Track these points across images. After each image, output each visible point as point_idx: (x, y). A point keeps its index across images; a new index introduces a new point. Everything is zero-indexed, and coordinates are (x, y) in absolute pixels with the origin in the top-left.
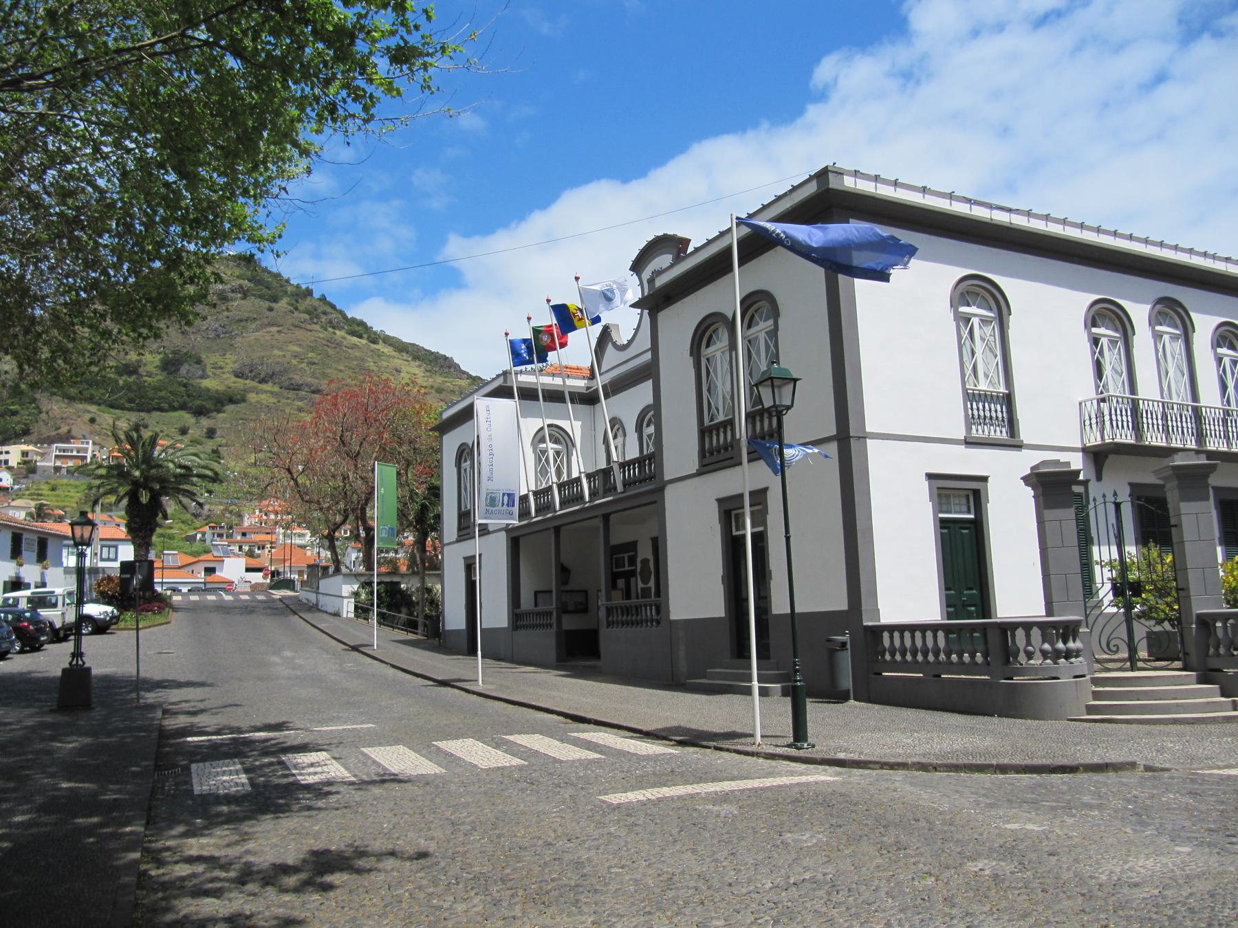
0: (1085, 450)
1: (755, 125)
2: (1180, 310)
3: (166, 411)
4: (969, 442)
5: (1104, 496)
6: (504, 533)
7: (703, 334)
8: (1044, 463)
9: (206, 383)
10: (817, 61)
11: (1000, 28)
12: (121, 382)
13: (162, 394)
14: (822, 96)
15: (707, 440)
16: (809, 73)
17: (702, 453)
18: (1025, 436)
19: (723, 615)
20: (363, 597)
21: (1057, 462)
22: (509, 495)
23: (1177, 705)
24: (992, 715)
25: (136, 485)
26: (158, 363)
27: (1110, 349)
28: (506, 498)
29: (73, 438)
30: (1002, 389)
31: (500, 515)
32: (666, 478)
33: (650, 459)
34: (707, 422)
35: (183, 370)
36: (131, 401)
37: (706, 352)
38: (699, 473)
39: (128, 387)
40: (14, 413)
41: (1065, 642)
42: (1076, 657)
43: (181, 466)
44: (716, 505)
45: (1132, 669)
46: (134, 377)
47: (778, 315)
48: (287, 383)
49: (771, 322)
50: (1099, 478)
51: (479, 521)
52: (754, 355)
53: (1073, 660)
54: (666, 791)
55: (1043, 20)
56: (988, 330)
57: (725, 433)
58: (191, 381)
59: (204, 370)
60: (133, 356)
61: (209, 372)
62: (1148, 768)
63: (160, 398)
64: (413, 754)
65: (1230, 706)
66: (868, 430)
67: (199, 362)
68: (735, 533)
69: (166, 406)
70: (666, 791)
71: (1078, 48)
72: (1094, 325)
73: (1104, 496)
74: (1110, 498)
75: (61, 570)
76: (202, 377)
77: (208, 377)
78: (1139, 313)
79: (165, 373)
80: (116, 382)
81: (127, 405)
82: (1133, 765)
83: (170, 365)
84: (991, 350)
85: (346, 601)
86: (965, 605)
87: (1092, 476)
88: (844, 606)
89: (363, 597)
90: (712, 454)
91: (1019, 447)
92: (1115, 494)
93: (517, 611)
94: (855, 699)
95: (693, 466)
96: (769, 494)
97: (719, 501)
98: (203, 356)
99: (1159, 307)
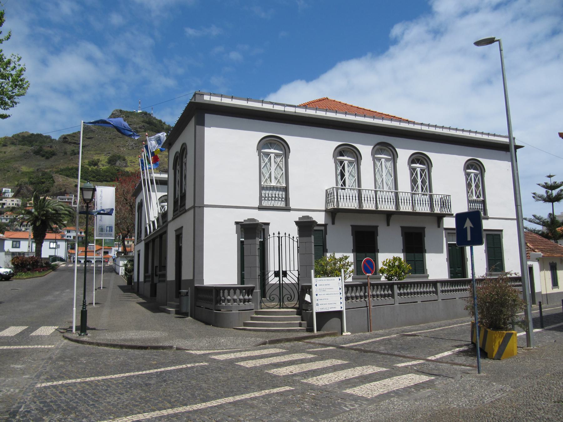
0: (327, 211)
1: (365, 54)
2: (391, 148)
3: (109, 182)
4: (261, 208)
5: (274, 234)
8: (304, 217)
9: (127, 169)
10: (392, 27)
11: (477, 10)
12: (90, 169)
13: (107, 174)
14: (395, 42)
16: (389, 32)
18: (292, 205)
20: (129, 266)
21: (308, 217)
22: (110, 227)
23: (274, 324)
24: (210, 325)
25: (36, 219)
26: (106, 160)
27: (348, 166)
28: (108, 228)
29: (67, 194)
30: (284, 185)
31: (107, 235)
35: (118, 163)
36: (94, 177)
39: (93, 171)
40: (43, 183)
41: (248, 296)
42: (248, 302)
43: (54, 210)
45: (279, 308)
46: (96, 167)
48: (162, 169)
50: (333, 223)
51: (96, 238)
53: (247, 303)
55: (497, 7)
56: (278, 160)
58: (121, 168)
59: (126, 163)
60: (96, 158)
61: (129, 164)
62: (178, 349)
63: (107, 176)
65: (298, 325)
66: (205, 203)
67: (124, 160)
69: (109, 179)
71: (514, 20)
72: (342, 155)
73: (274, 234)
74: (277, 235)
75: (4, 253)
76: (126, 166)
77: (128, 166)
78: (366, 150)
79: (109, 165)
80: (88, 169)
81: (92, 179)
82: (171, 347)
83: (112, 161)
84: (280, 168)
85: (121, 268)
86: (457, 273)
87: (330, 223)
89: (129, 266)
91: (289, 210)
92: (279, 233)
93: (147, 274)
94: (191, 316)
98: (126, 157)
99: (378, 147)
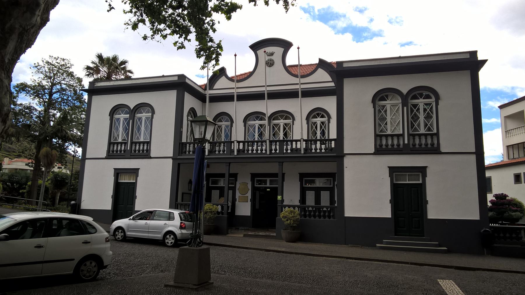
33: (224, 144)
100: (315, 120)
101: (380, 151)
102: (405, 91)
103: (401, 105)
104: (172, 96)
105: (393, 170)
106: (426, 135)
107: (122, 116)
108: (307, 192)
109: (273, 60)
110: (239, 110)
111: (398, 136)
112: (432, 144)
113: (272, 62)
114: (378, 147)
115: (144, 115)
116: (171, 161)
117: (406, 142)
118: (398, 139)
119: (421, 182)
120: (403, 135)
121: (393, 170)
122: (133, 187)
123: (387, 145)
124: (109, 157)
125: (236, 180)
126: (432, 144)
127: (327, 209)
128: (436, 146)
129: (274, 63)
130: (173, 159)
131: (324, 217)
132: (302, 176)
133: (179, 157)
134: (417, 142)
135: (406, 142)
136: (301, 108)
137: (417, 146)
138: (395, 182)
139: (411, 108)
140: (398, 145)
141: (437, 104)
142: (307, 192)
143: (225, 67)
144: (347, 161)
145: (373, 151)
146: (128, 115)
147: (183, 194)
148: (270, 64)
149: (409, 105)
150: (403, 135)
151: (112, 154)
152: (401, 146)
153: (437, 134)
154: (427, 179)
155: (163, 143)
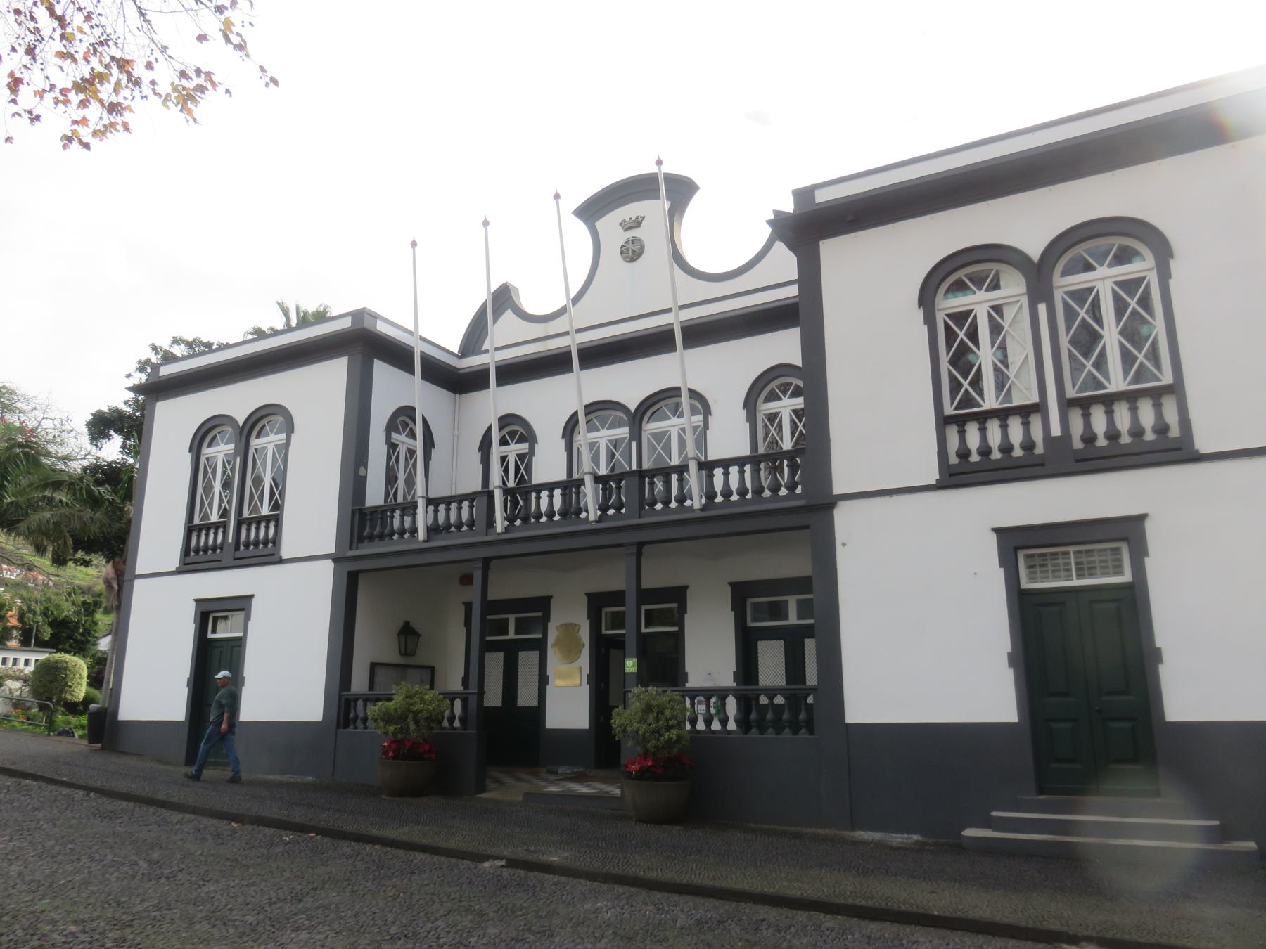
6: (285, 554)
7: (205, 434)
15: (194, 539)
17: (186, 551)
19: (183, 718)
32: (838, 489)
33: (472, 501)
34: (197, 521)
37: (207, 452)
38: (179, 572)
44: (194, 603)
47: (293, 432)
49: (284, 436)
52: (258, 462)
54: (1176, 844)
57: (216, 534)
64: (274, 816)
68: (210, 636)
70: (1176, 844)
88: (535, 703)
90: (197, 552)
95: (174, 562)
96: (254, 600)
97: (197, 601)
100: (772, 407)
101: (958, 474)
102: (1034, 248)
103: (1024, 301)
104: (332, 376)
105: (1014, 542)
106: (1131, 398)
107: (220, 451)
108: (762, 645)
109: (640, 241)
110: (546, 404)
111: (1025, 412)
112: (1161, 429)
113: (636, 247)
114: (953, 460)
115: (267, 442)
116: (329, 566)
117: (1056, 430)
118: (1026, 424)
119: (1126, 577)
120: (1038, 408)
121: (1014, 542)
122: (235, 648)
123: (985, 451)
124: (187, 567)
125: (546, 618)
126: (1161, 429)
127: (771, 698)
128: (1175, 432)
129: (642, 248)
130: (337, 559)
131: (778, 726)
132: (741, 593)
133: (350, 553)
134: (1099, 422)
135: (1056, 430)
136: (725, 372)
137: (1102, 442)
138: (1026, 584)
139: (1067, 306)
140: (1028, 446)
141: (1164, 275)
142: (762, 645)
143: (513, 282)
144: (845, 520)
145: (931, 475)
146: (232, 446)
147: (373, 666)
148: (632, 252)
149: (1058, 296)
150: (1038, 408)
151: (194, 558)
152: (1040, 449)
153: (1176, 389)
154: (1150, 564)
155: (312, 518)
